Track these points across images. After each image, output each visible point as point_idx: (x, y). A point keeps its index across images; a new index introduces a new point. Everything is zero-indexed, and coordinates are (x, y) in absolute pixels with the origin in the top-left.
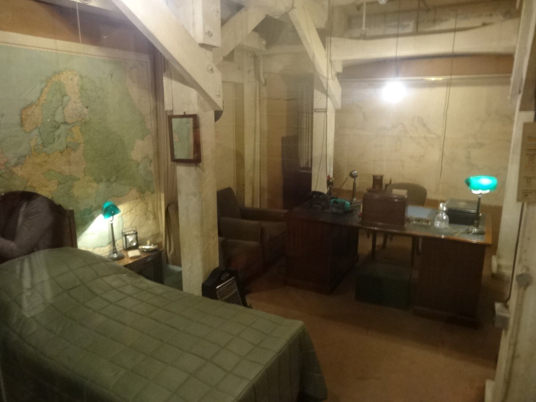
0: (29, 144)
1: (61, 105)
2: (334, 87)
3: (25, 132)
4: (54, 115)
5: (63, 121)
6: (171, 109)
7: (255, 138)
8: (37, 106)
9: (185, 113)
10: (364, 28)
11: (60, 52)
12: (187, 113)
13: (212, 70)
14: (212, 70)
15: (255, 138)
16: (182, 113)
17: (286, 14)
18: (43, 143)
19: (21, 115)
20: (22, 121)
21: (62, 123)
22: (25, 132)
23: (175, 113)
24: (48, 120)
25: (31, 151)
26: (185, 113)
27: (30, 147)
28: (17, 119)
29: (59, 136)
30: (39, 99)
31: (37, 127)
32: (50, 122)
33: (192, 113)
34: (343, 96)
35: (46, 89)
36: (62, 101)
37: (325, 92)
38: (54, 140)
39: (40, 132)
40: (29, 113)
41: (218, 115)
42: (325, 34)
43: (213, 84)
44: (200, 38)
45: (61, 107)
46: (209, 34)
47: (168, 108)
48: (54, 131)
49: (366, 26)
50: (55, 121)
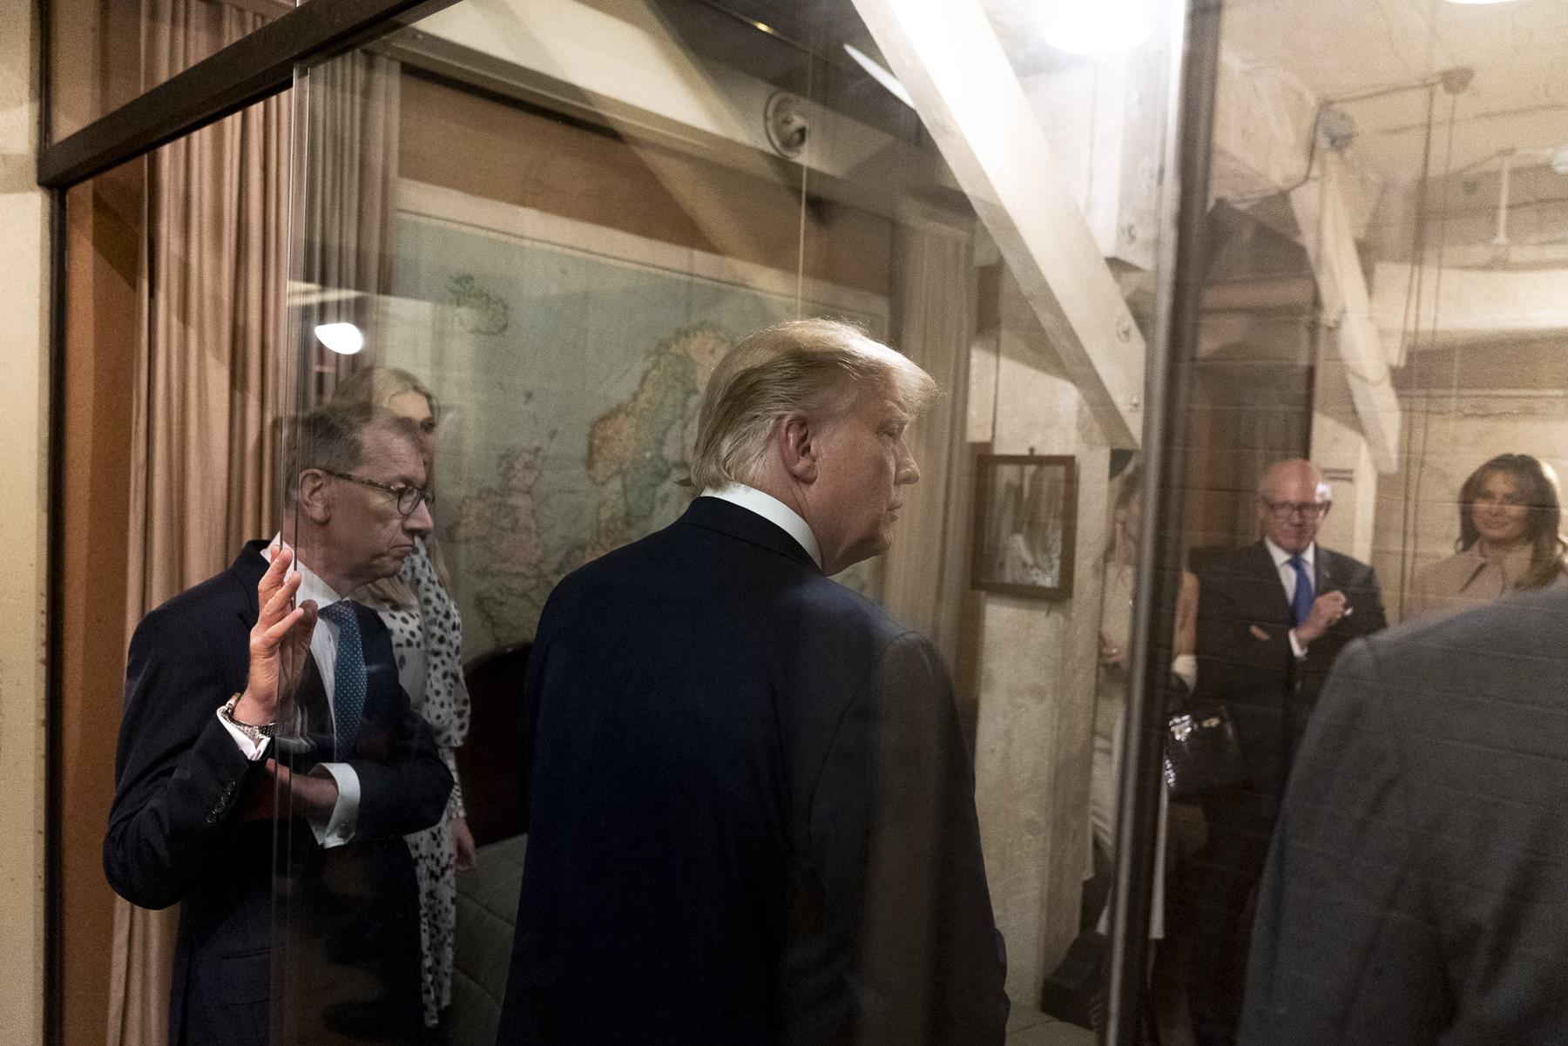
0: (598, 513)
1: (682, 417)
2: (1382, 404)
3: (594, 481)
4: (661, 443)
5: (677, 458)
6: (986, 437)
7: (1416, 519)
8: (628, 415)
9: (1032, 450)
10: (1501, 238)
11: (696, 280)
12: (1037, 452)
13: (1127, 333)
14: (1127, 333)
15: (1416, 519)
16: (1025, 452)
17: (1284, 196)
18: (628, 514)
19: (591, 436)
20: (591, 453)
21: (676, 465)
22: (594, 481)
23: (999, 450)
24: (648, 455)
25: (598, 532)
26: (1032, 450)
27: (599, 521)
28: (581, 447)
29: (665, 499)
30: (635, 397)
31: (620, 472)
32: (651, 459)
33: (1057, 449)
34: (1408, 431)
35: (654, 372)
36: (684, 406)
37: (1353, 419)
38: (652, 508)
39: (624, 486)
40: (609, 432)
41: (1119, 458)
42: (1368, 253)
43: (1124, 367)
44: (1108, 247)
45: (679, 422)
46: (1129, 233)
47: (977, 432)
48: (654, 486)
49: (1509, 234)
50: (661, 458)
